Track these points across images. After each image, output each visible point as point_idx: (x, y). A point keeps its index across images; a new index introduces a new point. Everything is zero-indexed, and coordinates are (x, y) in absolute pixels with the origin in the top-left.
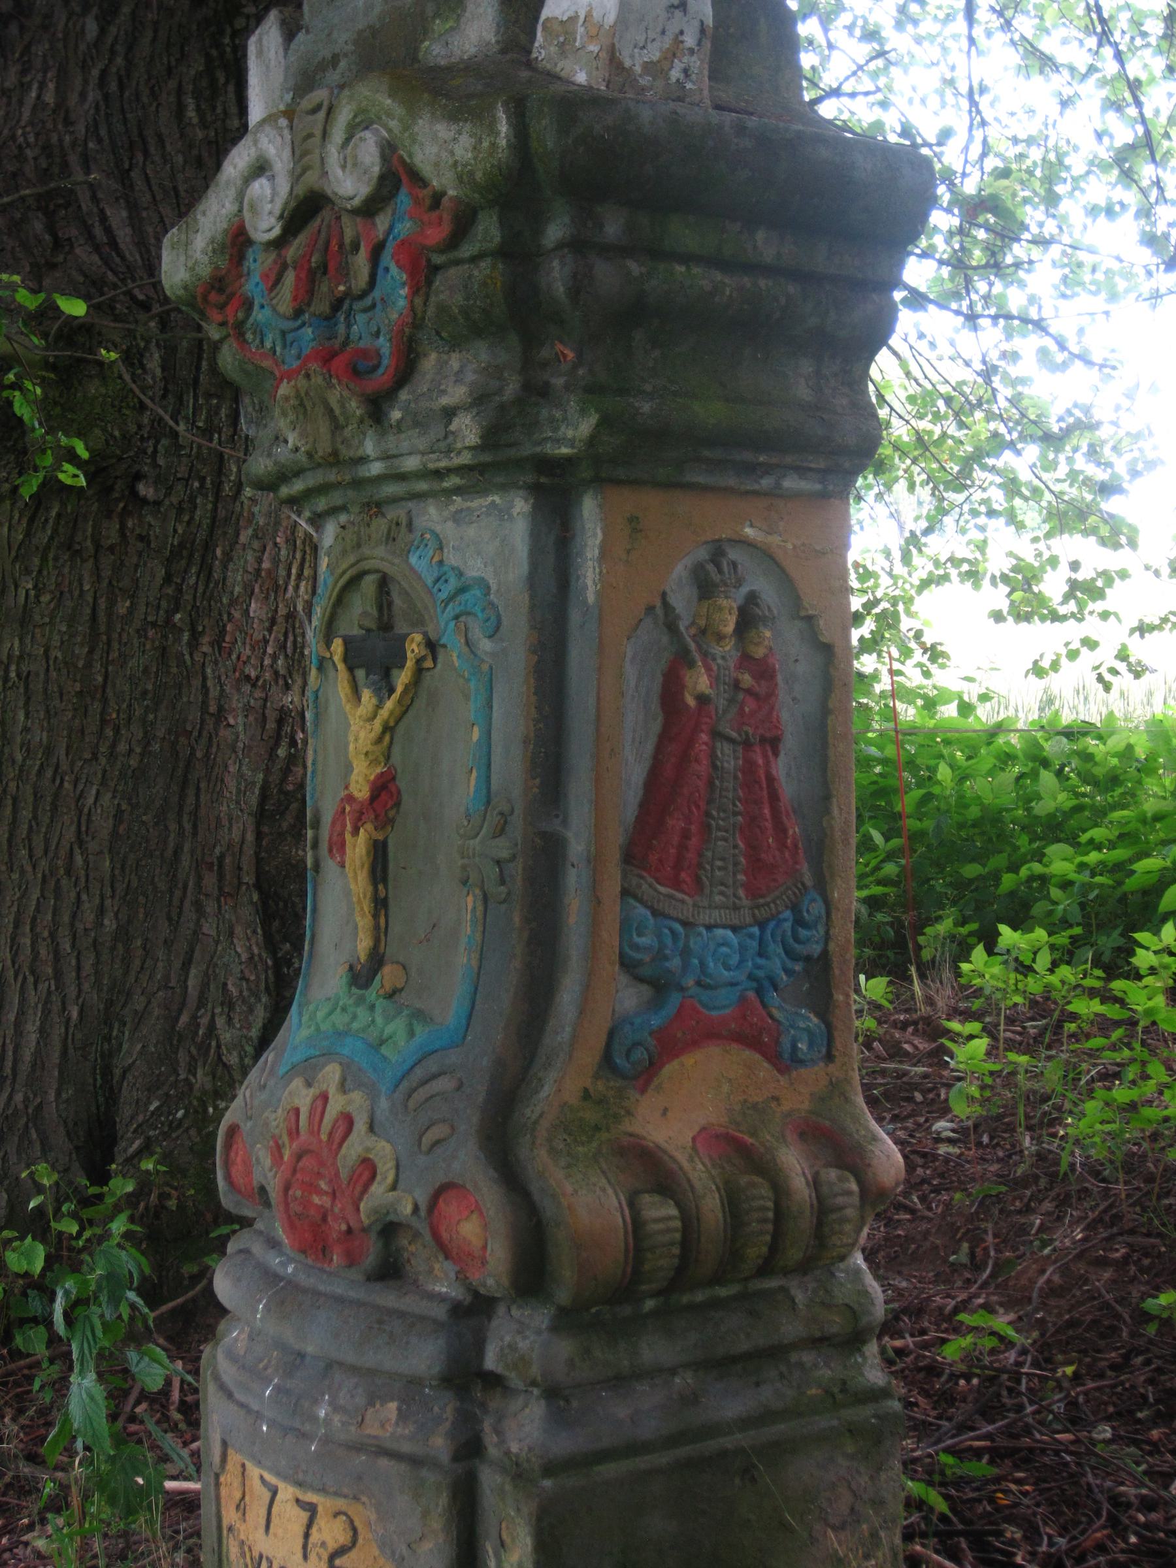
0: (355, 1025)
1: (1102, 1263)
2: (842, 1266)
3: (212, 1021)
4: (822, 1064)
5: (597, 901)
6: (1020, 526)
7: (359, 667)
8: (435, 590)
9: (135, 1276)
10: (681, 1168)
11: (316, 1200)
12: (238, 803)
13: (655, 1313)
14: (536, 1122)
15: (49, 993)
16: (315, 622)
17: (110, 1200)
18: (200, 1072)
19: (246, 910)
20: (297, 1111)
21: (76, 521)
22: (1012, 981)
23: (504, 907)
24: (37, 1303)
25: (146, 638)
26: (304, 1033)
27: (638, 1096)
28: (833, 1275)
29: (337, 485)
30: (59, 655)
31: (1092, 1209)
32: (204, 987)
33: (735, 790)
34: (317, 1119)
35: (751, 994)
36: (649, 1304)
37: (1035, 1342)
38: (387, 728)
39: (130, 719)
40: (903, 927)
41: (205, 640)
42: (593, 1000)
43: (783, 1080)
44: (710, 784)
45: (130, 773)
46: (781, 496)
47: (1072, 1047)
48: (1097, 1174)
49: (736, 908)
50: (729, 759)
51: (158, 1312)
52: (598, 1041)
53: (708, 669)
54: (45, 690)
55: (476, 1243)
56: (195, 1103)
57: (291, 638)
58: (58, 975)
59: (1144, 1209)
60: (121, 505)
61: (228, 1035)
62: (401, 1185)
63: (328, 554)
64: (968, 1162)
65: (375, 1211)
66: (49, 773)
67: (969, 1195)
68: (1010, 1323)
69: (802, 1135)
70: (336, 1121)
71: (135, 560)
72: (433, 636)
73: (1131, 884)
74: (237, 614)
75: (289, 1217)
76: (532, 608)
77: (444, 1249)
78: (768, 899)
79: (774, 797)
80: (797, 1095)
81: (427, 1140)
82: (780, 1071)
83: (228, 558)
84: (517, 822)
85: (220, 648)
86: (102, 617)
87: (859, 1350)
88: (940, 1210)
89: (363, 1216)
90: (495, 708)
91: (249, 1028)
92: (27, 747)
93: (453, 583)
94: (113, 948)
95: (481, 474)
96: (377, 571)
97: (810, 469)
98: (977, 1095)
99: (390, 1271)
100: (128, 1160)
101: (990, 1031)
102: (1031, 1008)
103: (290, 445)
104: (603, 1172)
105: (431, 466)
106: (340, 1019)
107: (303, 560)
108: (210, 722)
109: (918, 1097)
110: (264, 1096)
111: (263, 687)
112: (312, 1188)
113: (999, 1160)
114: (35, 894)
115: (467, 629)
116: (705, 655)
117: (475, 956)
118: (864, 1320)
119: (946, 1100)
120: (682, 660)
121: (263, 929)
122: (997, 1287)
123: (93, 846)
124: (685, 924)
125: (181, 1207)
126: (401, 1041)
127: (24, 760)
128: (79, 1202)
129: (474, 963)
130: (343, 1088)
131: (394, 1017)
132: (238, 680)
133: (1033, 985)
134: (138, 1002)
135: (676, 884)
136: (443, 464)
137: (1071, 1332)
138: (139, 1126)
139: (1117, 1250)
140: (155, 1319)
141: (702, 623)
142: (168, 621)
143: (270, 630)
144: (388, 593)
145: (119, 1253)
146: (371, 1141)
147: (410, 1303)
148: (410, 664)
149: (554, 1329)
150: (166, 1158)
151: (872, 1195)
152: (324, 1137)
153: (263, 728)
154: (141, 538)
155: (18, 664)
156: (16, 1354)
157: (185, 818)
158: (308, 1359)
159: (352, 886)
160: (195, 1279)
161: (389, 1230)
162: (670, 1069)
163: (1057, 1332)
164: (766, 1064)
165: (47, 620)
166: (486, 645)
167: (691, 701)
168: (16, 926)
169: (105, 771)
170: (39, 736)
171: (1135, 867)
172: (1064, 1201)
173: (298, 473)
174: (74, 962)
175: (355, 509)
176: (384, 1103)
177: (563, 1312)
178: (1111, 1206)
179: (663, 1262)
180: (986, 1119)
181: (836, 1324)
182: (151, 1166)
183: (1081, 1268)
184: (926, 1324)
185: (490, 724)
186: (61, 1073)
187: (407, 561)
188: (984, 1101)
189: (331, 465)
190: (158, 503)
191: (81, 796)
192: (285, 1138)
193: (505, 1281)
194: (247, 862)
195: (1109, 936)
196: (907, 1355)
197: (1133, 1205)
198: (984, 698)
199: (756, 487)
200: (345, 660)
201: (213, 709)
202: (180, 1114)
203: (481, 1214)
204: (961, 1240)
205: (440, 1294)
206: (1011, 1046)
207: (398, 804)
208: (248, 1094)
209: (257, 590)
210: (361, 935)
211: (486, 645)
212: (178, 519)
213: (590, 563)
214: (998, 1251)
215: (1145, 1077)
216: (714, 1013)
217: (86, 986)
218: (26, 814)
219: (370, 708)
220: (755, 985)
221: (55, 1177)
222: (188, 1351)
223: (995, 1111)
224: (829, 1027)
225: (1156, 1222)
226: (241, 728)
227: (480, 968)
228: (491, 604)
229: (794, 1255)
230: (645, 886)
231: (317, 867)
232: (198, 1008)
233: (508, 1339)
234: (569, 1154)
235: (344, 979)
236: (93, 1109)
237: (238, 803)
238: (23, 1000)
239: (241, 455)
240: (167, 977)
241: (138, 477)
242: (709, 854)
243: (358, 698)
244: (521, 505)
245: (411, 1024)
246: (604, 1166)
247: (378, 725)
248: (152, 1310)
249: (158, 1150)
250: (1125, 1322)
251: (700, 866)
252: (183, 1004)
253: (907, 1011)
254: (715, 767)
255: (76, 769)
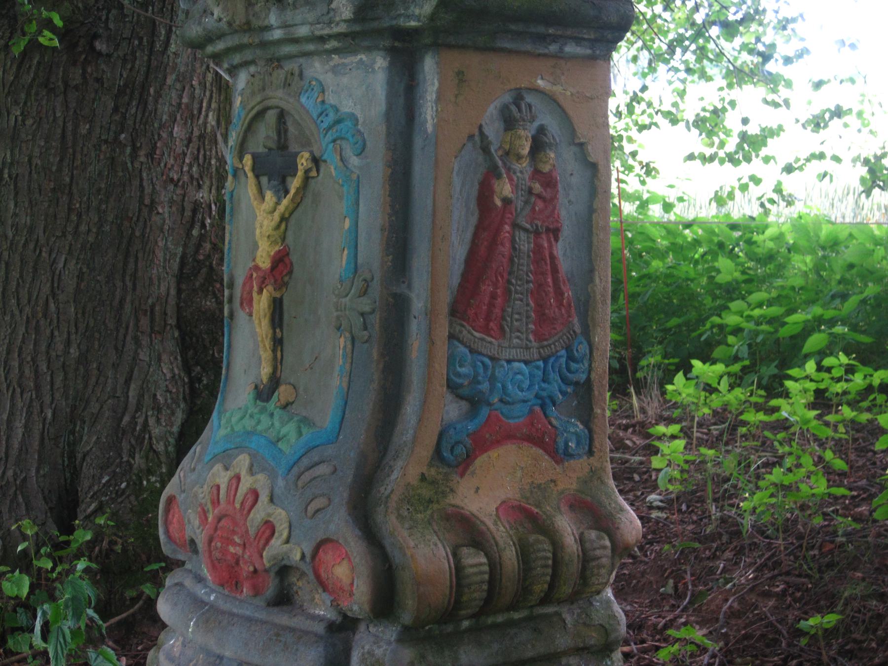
0: (259, 428)
1: (767, 595)
2: (597, 598)
3: (146, 420)
4: (585, 457)
5: (431, 342)
6: (709, 79)
7: (263, 175)
8: (319, 122)
9: (93, 599)
10: (488, 529)
11: (232, 549)
12: (164, 267)
13: (469, 630)
14: (388, 496)
15: (31, 400)
16: (231, 142)
17: (74, 546)
18: (137, 456)
19: (170, 344)
20: (218, 487)
21: (51, 67)
22: (702, 398)
23: (366, 346)
24: (24, 617)
25: (100, 151)
26: (222, 432)
27: (458, 478)
28: (591, 604)
29: (248, 46)
30: (39, 162)
31: (760, 557)
32: (141, 396)
33: (528, 265)
34: (233, 493)
35: (537, 409)
36: (466, 624)
37: (721, 649)
38: (283, 219)
39: (89, 207)
40: (625, 359)
41: (142, 153)
42: (430, 410)
43: (559, 469)
44: (511, 260)
45: (88, 246)
46: (561, 58)
47: (743, 444)
48: (762, 533)
49: (527, 348)
50: (525, 243)
51: (108, 624)
52: (430, 440)
53: (511, 180)
54: (29, 187)
55: (346, 581)
56: (134, 478)
57: (202, 152)
58: (38, 387)
59: (796, 558)
60: (83, 56)
61: (157, 430)
62: (292, 540)
63: (242, 94)
64: (672, 523)
65: (274, 558)
66: (32, 246)
67: (674, 546)
68: (704, 636)
69: (572, 507)
70: (246, 494)
71: (92, 96)
72: (317, 154)
73: (784, 332)
74: (164, 135)
75: (212, 561)
76: (388, 134)
77: (323, 584)
78: (550, 342)
79: (555, 271)
80: (568, 478)
81: (311, 509)
82: (557, 462)
83: (158, 95)
84: (376, 285)
85: (152, 159)
86: (69, 133)
87: (609, 656)
88: (652, 557)
89: (265, 560)
90: (361, 205)
91: (172, 426)
92: (16, 227)
93: (332, 117)
94: (77, 369)
95: (353, 39)
96: (277, 107)
97: (584, 39)
98: (678, 476)
99: (283, 599)
100: (87, 517)
101: (686, 433)
102: (714, 416)
103: (215, 16)
104: (435, 532)
105: (318, 33)
106: (248, 423)
107: (211, 97)
108: (145, 211)
109: (637, 477)
110: (193, 476)
111: (183, 187)
112: (229, 541)
113: (694, 522)
114: (22, 330)
115: (341, 150)
116: (509, 170)
117: (346, 380)
118: (613, 636)
119: (656, 480)
120: (493, 173)
121: (181, 356)
122: (694, 610)
123: (62, 297)
124: (492, 359)
125: (125, 550)
126: (292, 438)
127: (14, 236)
128: (52, 546)
129: (345, 385)
130: (251, 471)
131: (288, 422)
132: (165, 182)
133: (716, 401)
134: (94, 407)
135: (486, 330)
136: (326, 31)
137: (746, 643)
138: (95, 494)
139: (778, 586)
140: (107, 628)
141: (507, 147)
142: (116, 139)
143: (187, 146)
144: (285, 123)
145: (79, 579)
146: (271, 509)
147: (298, 622)
148: (300, 173)
149: (400, 640)
150: (114, 516)
151: (620, 549)
152: (238, 506)
153: (183, 215)
154: (97, 80)
155: (9, 169)
156: (9, 653)
157: (128, 278)
158: (225, 660)
159: (258, 330)
160: (134, 600)
161: (284, 571)
162: (481, 460)
163: (736, 642)
164: (546, 457)
165: (30, 137)
166: (354, 161)
167: (499, 203)
168: (8, 353)
169: (71, 245)
170: (25, 220)
171: (788, 319)
172: (739, 552)
173: (221, 36)
174: (49, 378)
175: (262, 63)
176: (281, 483)
177: (406, 629)
178: (773, 555)
179: (475, 595)
180: (684, 493)
181: (594, 638)
182: (102, 522)
183: (753, 598)
184: (645, 636)
185: (358, 217)
186: (39, 457)
187: (299, 101)
188: (683, 481)
189: (245, 31)
190: (109, 56)
191: (54, 262)
192: (209, 506)
193: (367, 607)
194: (171, 310)
195: (768, 367)
196: (632, 657)
197: (789, 555)
198: (681, 199)
199: (546, 51)
200: (253, 169)
201: (147, 201)
202: (123, 485)
203: (350, 560)
204: (667, 577)
205: (319, 616)
206: (701, 443)
207: (291, 272)
208: (182, 475)
209: (178, 118)
210: (264, 364)
211: (354, 161)
212: (123, 67)
213: (429, 104)
214: (694, 585)
215: (799, 466)
216: (511, 421)
217: (57, 395)
218: (15, 274)
219: (272, 204)
220: (539, 402)
221: (36, 529)
222: (130, 651)
223: (691, 488)
224: (590, 431)
225: (805, 567)
226: (167, 215)
227: (348, 389)
228: (359, 131)
229: (566, 590)
230: (465, 332)
231: (232, 316)
232: (136, 412)
233: (367, 647)
234: (411, 519)
235: (252, 396)
236: (62, 481)
237: (164, 267)
238: (13, 405)
239: (168, 22)
240: (114, 389)
241: (95, 36)
242: (510, 310)
243: (263, 198)
244: (381, 62)
245: (299, 427)
246: (436, 528)
247: (277, 216)
248: (104, 622)
249: (108, 510)
250: (783, 637)
251: (503, 318)
252: (126, 408)
253: (627, 417)
254: (514, 249)
255: (51, 243)
